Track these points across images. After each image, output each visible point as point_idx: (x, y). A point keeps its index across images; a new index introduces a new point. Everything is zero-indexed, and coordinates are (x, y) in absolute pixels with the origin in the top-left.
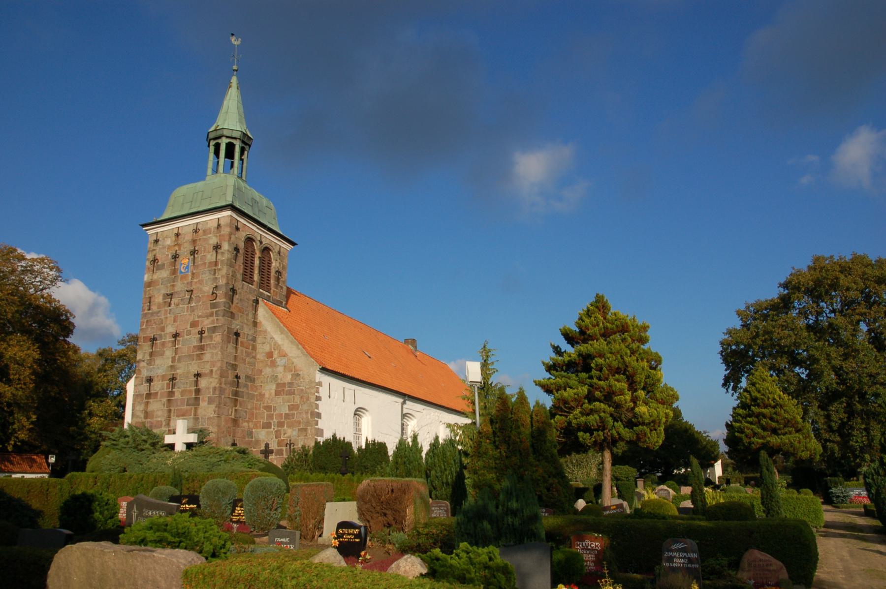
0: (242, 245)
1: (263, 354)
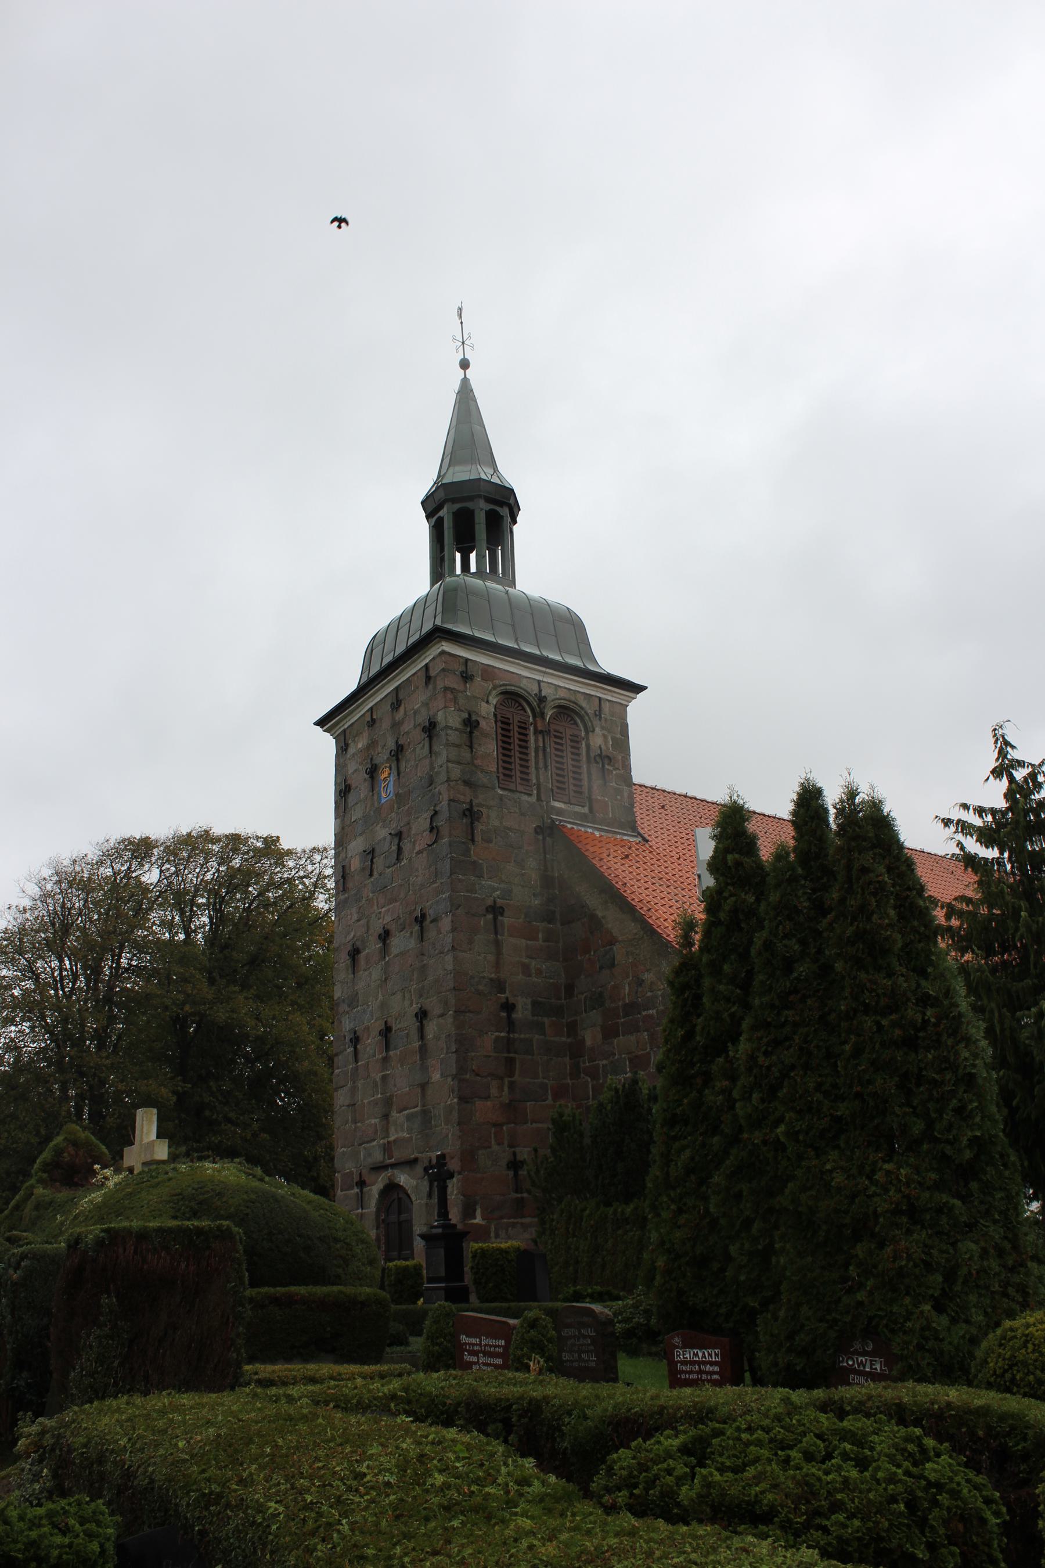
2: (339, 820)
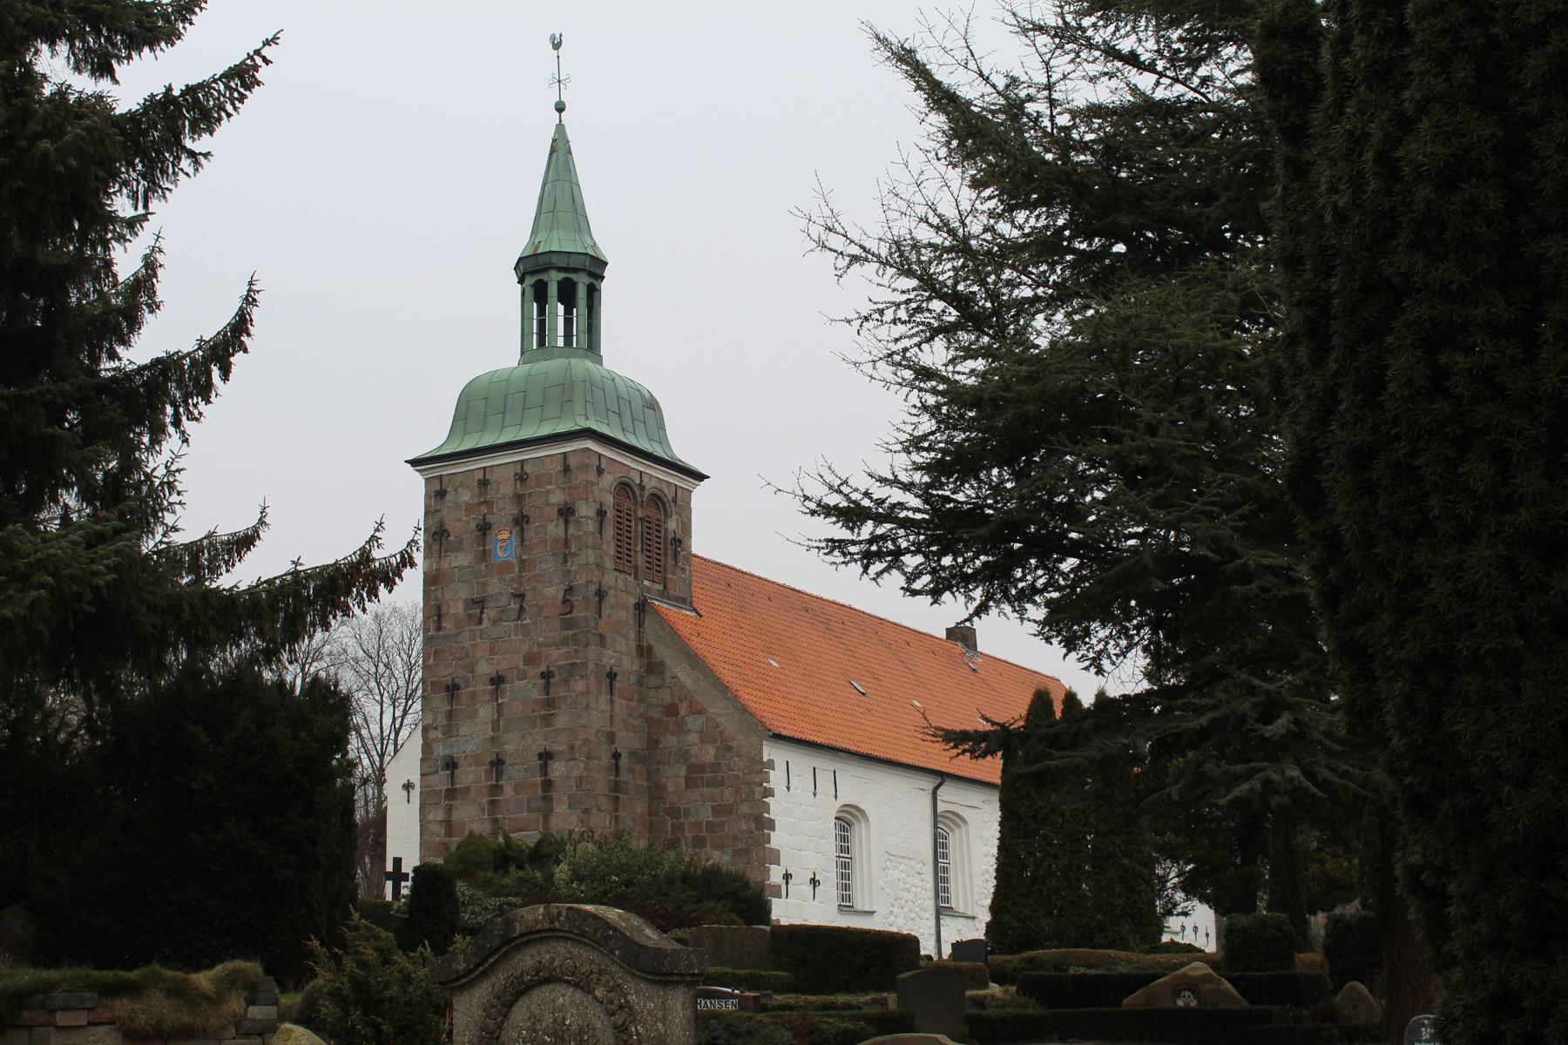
0: (609, 500)
1: (660, 709)
2: (428, 561)
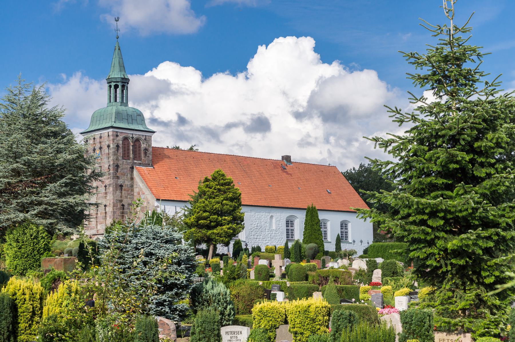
0: (121, 142)
